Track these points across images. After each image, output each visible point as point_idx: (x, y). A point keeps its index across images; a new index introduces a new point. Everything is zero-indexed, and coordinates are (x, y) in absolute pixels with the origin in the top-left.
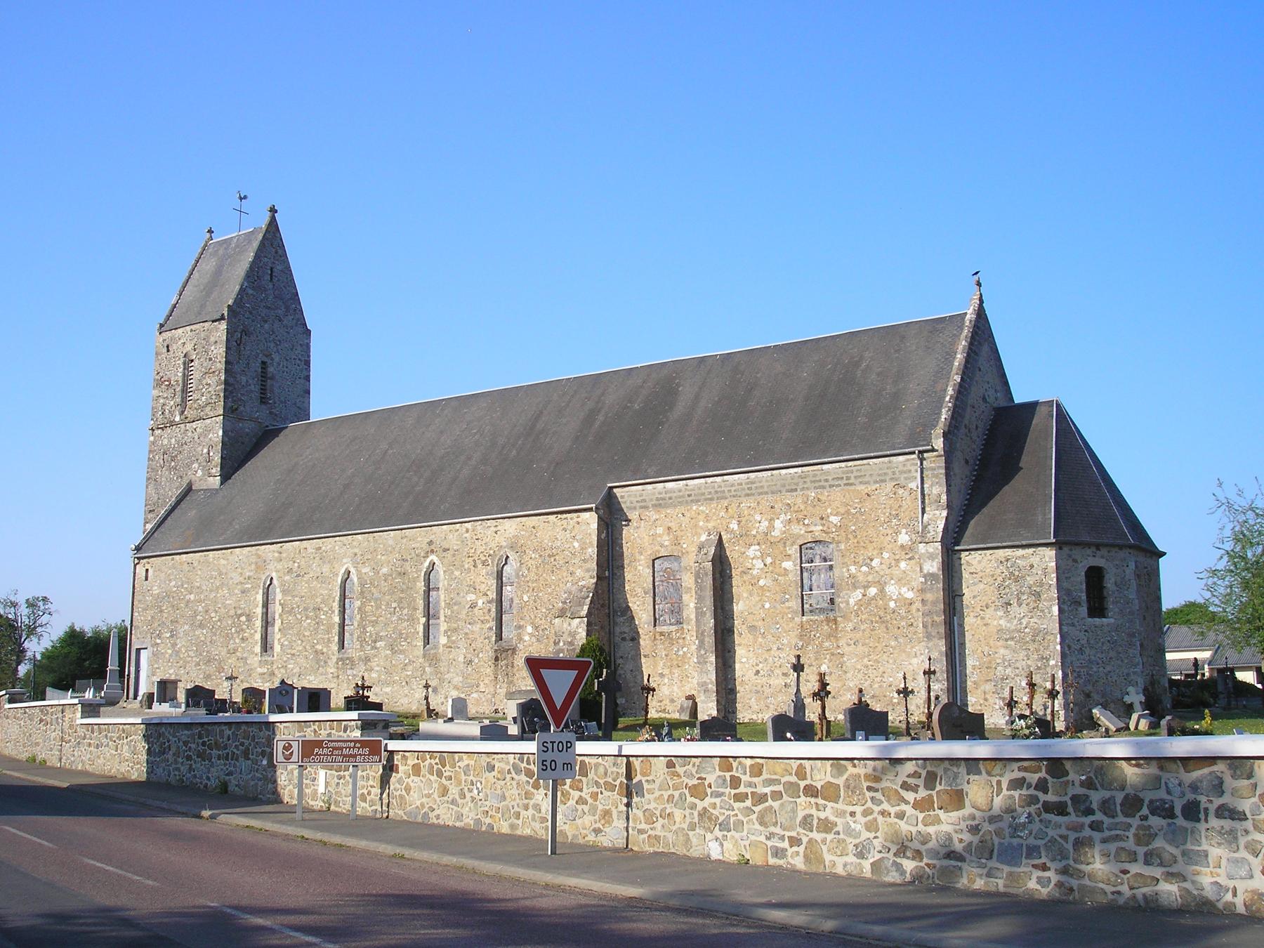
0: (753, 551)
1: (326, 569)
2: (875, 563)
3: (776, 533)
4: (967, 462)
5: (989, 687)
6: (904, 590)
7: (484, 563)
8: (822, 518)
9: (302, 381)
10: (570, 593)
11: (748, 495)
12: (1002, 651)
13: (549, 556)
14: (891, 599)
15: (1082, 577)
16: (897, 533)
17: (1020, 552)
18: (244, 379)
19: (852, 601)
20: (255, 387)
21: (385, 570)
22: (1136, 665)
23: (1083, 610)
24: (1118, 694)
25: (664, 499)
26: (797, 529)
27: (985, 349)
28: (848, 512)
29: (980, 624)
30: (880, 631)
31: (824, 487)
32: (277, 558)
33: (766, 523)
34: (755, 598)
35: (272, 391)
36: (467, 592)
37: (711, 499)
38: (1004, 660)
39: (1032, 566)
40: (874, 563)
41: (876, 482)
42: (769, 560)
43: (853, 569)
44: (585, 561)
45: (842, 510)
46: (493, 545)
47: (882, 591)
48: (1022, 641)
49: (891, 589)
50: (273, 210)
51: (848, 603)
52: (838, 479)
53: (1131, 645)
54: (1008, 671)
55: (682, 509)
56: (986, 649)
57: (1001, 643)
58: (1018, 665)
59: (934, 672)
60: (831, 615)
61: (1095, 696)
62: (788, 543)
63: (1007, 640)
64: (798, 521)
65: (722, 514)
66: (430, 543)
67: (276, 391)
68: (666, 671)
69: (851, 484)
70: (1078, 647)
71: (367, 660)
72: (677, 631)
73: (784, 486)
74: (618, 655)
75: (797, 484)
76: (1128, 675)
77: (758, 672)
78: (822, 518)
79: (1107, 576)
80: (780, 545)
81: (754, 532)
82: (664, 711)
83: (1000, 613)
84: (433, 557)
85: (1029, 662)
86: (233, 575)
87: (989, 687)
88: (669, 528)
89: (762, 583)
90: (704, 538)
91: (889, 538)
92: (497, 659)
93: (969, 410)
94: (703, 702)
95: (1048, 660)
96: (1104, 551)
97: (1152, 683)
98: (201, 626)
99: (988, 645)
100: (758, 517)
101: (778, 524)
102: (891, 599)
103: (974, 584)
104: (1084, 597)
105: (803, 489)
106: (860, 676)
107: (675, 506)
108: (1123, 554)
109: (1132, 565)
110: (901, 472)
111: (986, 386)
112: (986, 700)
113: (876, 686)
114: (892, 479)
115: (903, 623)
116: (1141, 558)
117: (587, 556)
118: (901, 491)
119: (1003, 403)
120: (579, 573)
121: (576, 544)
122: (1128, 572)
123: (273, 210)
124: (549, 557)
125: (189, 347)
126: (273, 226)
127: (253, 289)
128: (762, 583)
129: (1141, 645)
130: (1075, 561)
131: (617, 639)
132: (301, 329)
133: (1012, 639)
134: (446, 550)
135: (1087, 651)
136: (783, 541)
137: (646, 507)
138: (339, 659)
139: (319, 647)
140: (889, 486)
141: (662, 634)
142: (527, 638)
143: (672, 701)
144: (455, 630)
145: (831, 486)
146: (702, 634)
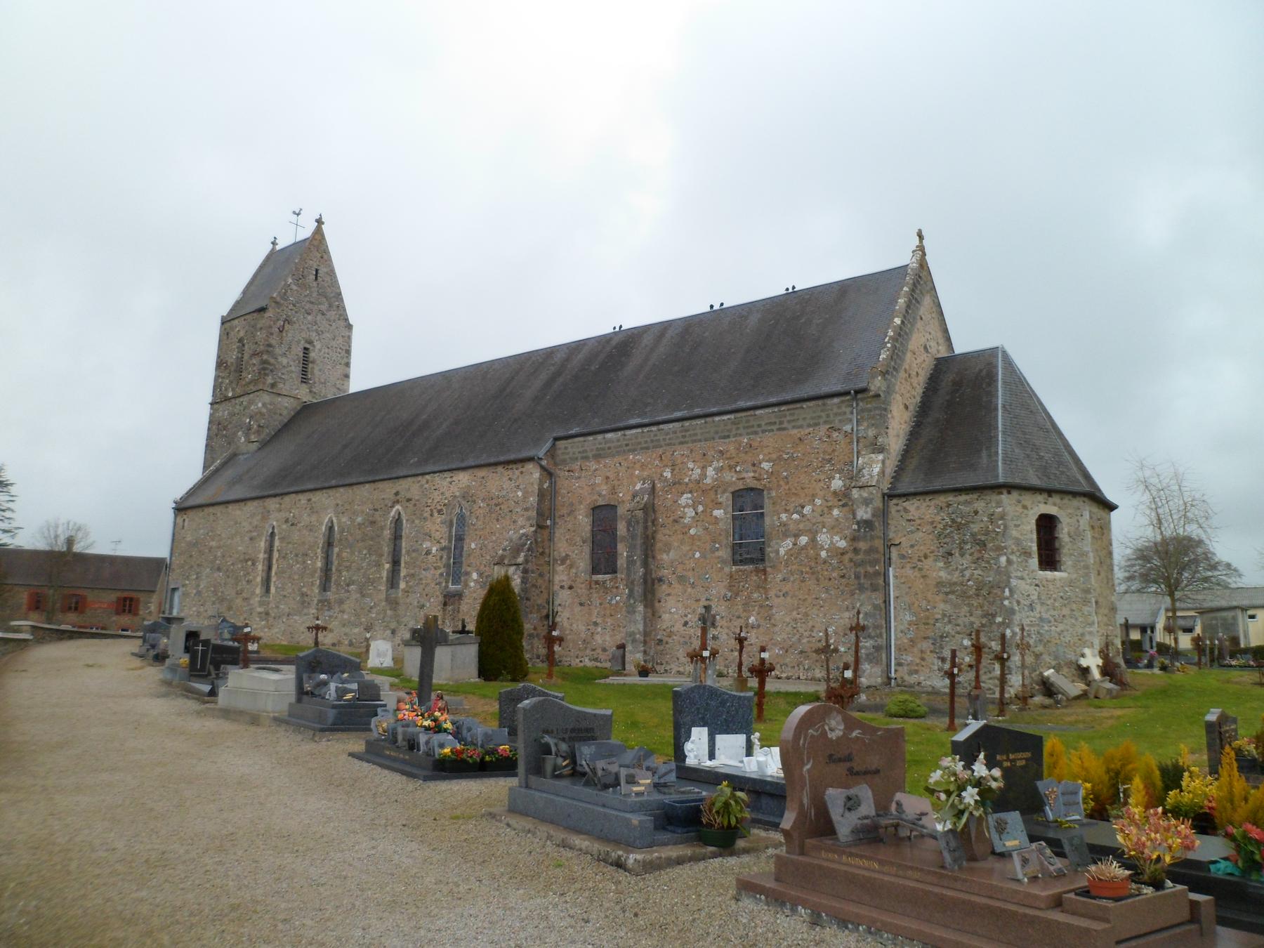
0: (685, 499)
1: (314, 518)
2: (807, 510)
3: (708, 481)
4: (906, 407)
5: (926, 645)
6: (837, 538)
7: (440, 512)
8: (754, 465)
9: (343, 367)
10: (511, 541)
11: (682, 443)
12: (942, 606)
13: (496, 505)
14: (822, 548)
15: (1032, 525)
16: (831, 478)
17: (963, 498)
18: (285, 361)
19: (782, 551)
20: (296, 369)
21: (359, 519)
22: (1092, 624)
23: (1034, 562)
24: (1071, 656)
25: (603, 449)
26: (729, 477)
27: (927, 301)
28: (780, 458)
29: (286, 399)
30: (811, 583)
31: (756, 433)
32: (277, 512)
33: (699, 471)
34: (685, 548)
35: (313, 373)
36: (430, 539)
37: (647, 448)
38: (944, 615)
39: (976, 513)
40: (805, 511)
41: (809, 426)
42: (700, 508)
43: (784, 516)
44: (526, 509)
45: (774, 456)
46: (448, 494)
47: (813, 540)
48: (964, 595)
49: (823, 538)
50: (319, 221)
51: (777, 552)
52: (771, 424)
53: (1086, 602)
54: (948, 628)
55: (617, 459)
56: (924, 603)
57: (941, 596)
58: (960, 622)
59: (863, 628)
60: (761, 567)
61: (1046, 658)
62: (720, 491)
63: (947, 594)
64: (730, 467)
65: (657, 462)
66: (397, 494)
67: (316, 371)
68: (599, 621)
69: (784, 429)
70: (1027, 603)
71: (341, 602)
72: (611, 580)
73: (717, 432)
74: (556, 603)
75: (730, 431)
76: (1083, 635)
77: (686, 624)
78: (754, 465)
79: (1059, 526)
80: (712, 493)
81: (687, 480)
82: (596, 660)
83: (941, 564)
84: (398, 507)
85: (972, 619)
86: (244, 524)
87: (926, 645)
88: (607, 478)
89: (692, 532)
90: (638, 487)
91: (822, 484)
92: (445, 604)
93: (909, 355)
94: (631, 652)
95: (994, 616)
96: (1056, 499)
97: (1107, 645)
98: (219, 569)
99: (925, 598)
100: (691, 465)
101: (710, 471)
102: (822, 548)
103: (912, 532)
104: (1035, 548)
105: (735, 436)
106: (789, 629)
107: (613, 456)
108: (1077, 502)
109: (1087, 515)
110: (836, 414)
111: (928, 336)
112: (923, 659)
113: (805, 641)
114: (825, 422)
115: (835, 575)
116: (1096, 509)
117: (529, 505)
118: (835, 434)
119: (943, 353)
120: (521, 521)
121: (520, 494)
122: (1082, 522)
123: (319, 221)
124: (496, 505)
125: (242, 334)
126: (319, 232)
127: (297, 285)
128: (692, 532)
129: (1097, 602)
130: (1025, 507)
131: (556, 587)
132: (342, 323)
133: (953, 592)
134: (409, 500)
135: (1038, 607)
136: (715, 489)
137: (586, 458)
138: (320, 601)
139: (304, 590)
140: (823, 429)
141: (597, 582)
142: (472, 584)
143: (604, 650)
144: (413, 575)
145: (764, 431)
146: (632, 583)
